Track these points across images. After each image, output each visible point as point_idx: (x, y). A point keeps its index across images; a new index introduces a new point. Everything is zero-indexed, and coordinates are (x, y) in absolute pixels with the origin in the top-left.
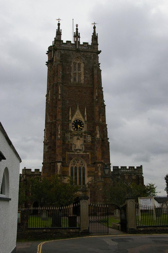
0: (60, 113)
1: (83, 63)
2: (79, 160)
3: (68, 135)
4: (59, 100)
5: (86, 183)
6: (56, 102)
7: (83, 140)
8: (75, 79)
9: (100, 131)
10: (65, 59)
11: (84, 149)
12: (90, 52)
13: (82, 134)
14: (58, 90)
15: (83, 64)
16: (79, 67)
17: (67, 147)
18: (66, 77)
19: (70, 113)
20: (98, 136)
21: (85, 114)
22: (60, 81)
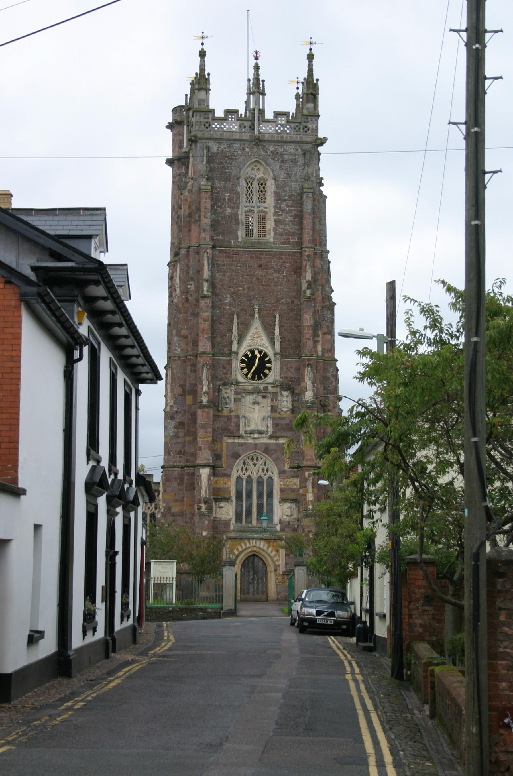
0: (207, 334)
1: (275, 179)
2: (257, 459)
3: (229, 393)
4: (205, 297)
5: (276, 520)
6: (197, 301)
7: (268, 406)
8: (249, 232)
9: (313, 383)
10: (220, 167)
11: (270, 430)
12: (293, 142)
13: (266, 388)
14: (200, 263)
15: (273, 182)
16: (262, 191)
17: (227, 426)
18: (222, 226)
19: (235, 332)
20: (309, 395)
21: (277, 332)
22: (206, 236)
